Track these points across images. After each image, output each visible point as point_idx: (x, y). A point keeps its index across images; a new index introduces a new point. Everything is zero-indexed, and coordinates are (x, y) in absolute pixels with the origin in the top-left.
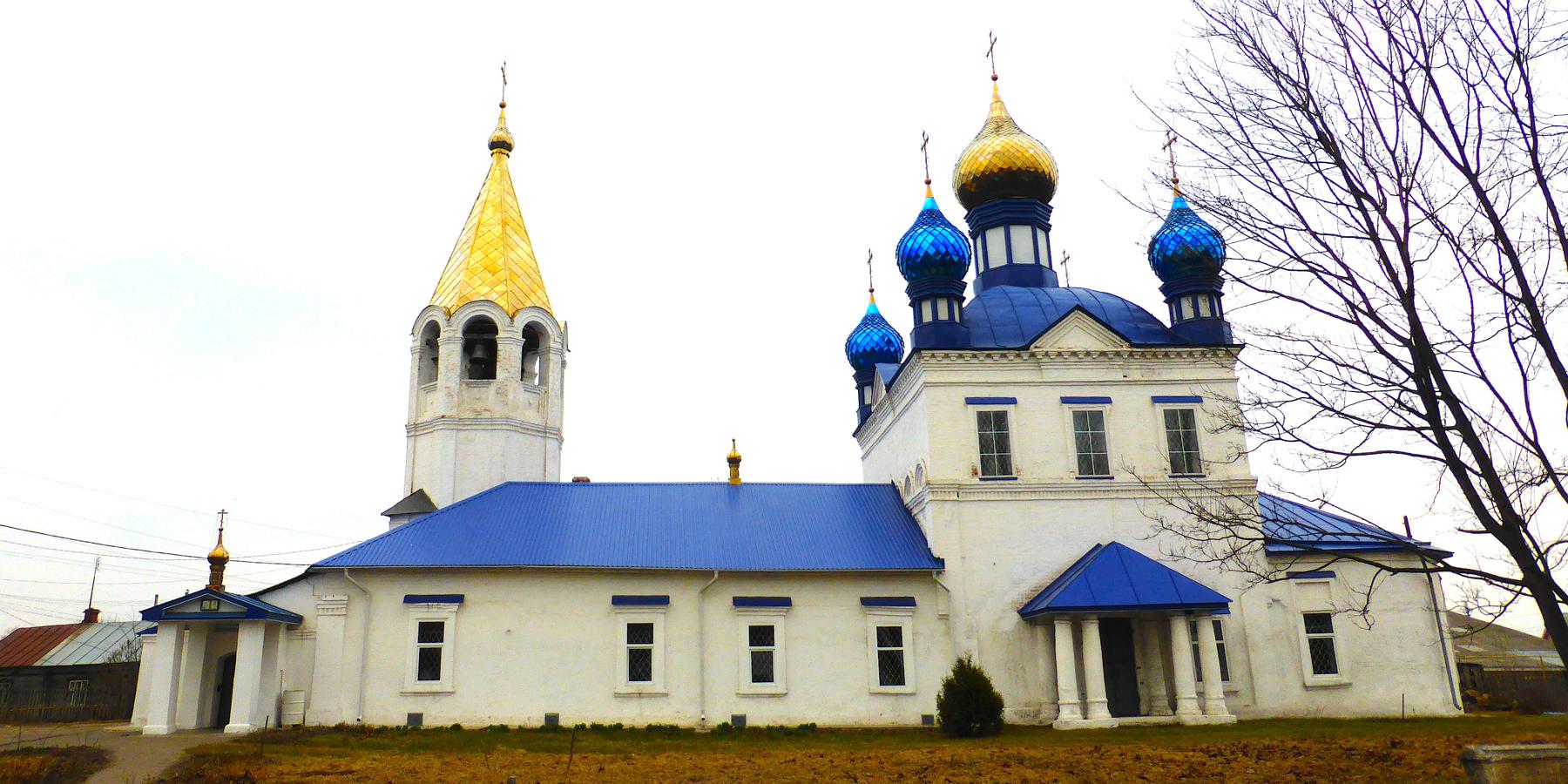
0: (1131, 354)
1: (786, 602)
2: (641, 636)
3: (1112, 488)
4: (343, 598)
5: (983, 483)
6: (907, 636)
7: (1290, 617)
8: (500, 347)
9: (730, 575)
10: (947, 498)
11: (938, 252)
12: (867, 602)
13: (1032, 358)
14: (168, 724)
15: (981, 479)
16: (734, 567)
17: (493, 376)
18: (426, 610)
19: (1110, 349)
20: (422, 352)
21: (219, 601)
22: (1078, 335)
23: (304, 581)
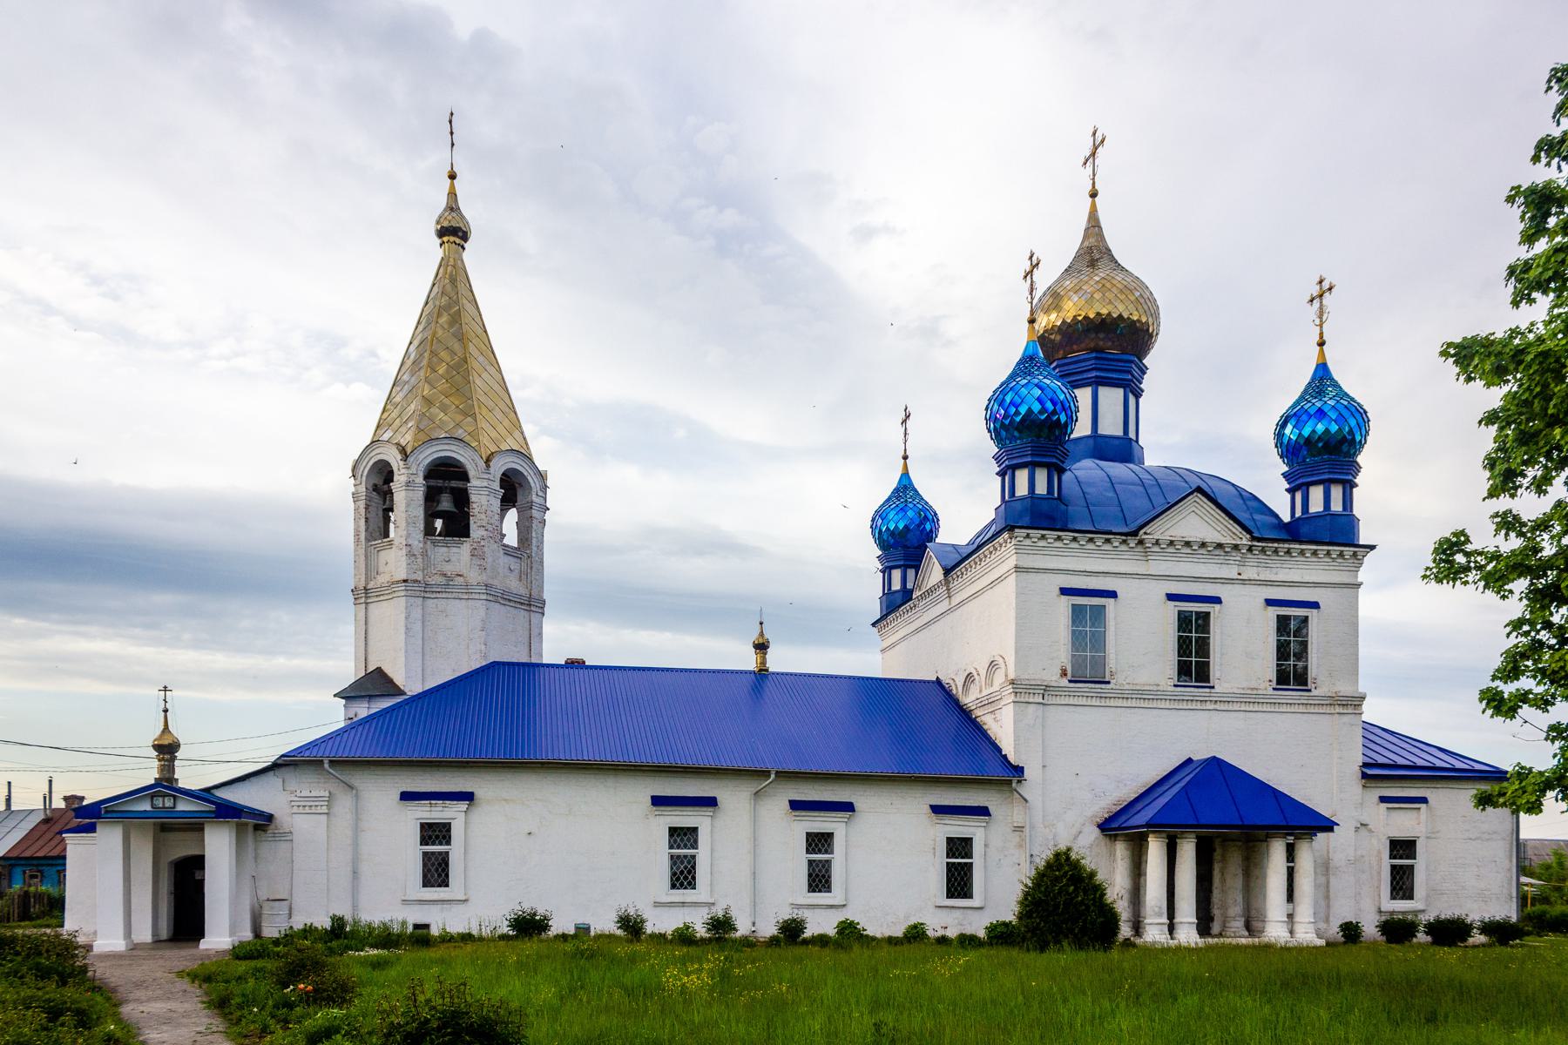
0: (1250, 549)
1: (848, 807)
2: (682, 840)
3: (1211, 699)
4: (322, 794)
5: (1072, 685)
6: (977, 848)
7: (1375, 841)
8: (473, 498)
9: (786, 776)
10: (1031, 700)
11: (1044, 410)
12: (938, 810)
13: (1139, 546)
14: (125, 939)
15: (1070, 681)
16: (792, 767)
17: (468, 536)
18: (428, 809)
19: (1228, 542)
20: (369, 500)
21: (174, 797)
22: (1195, 522)
23: (271, 773)
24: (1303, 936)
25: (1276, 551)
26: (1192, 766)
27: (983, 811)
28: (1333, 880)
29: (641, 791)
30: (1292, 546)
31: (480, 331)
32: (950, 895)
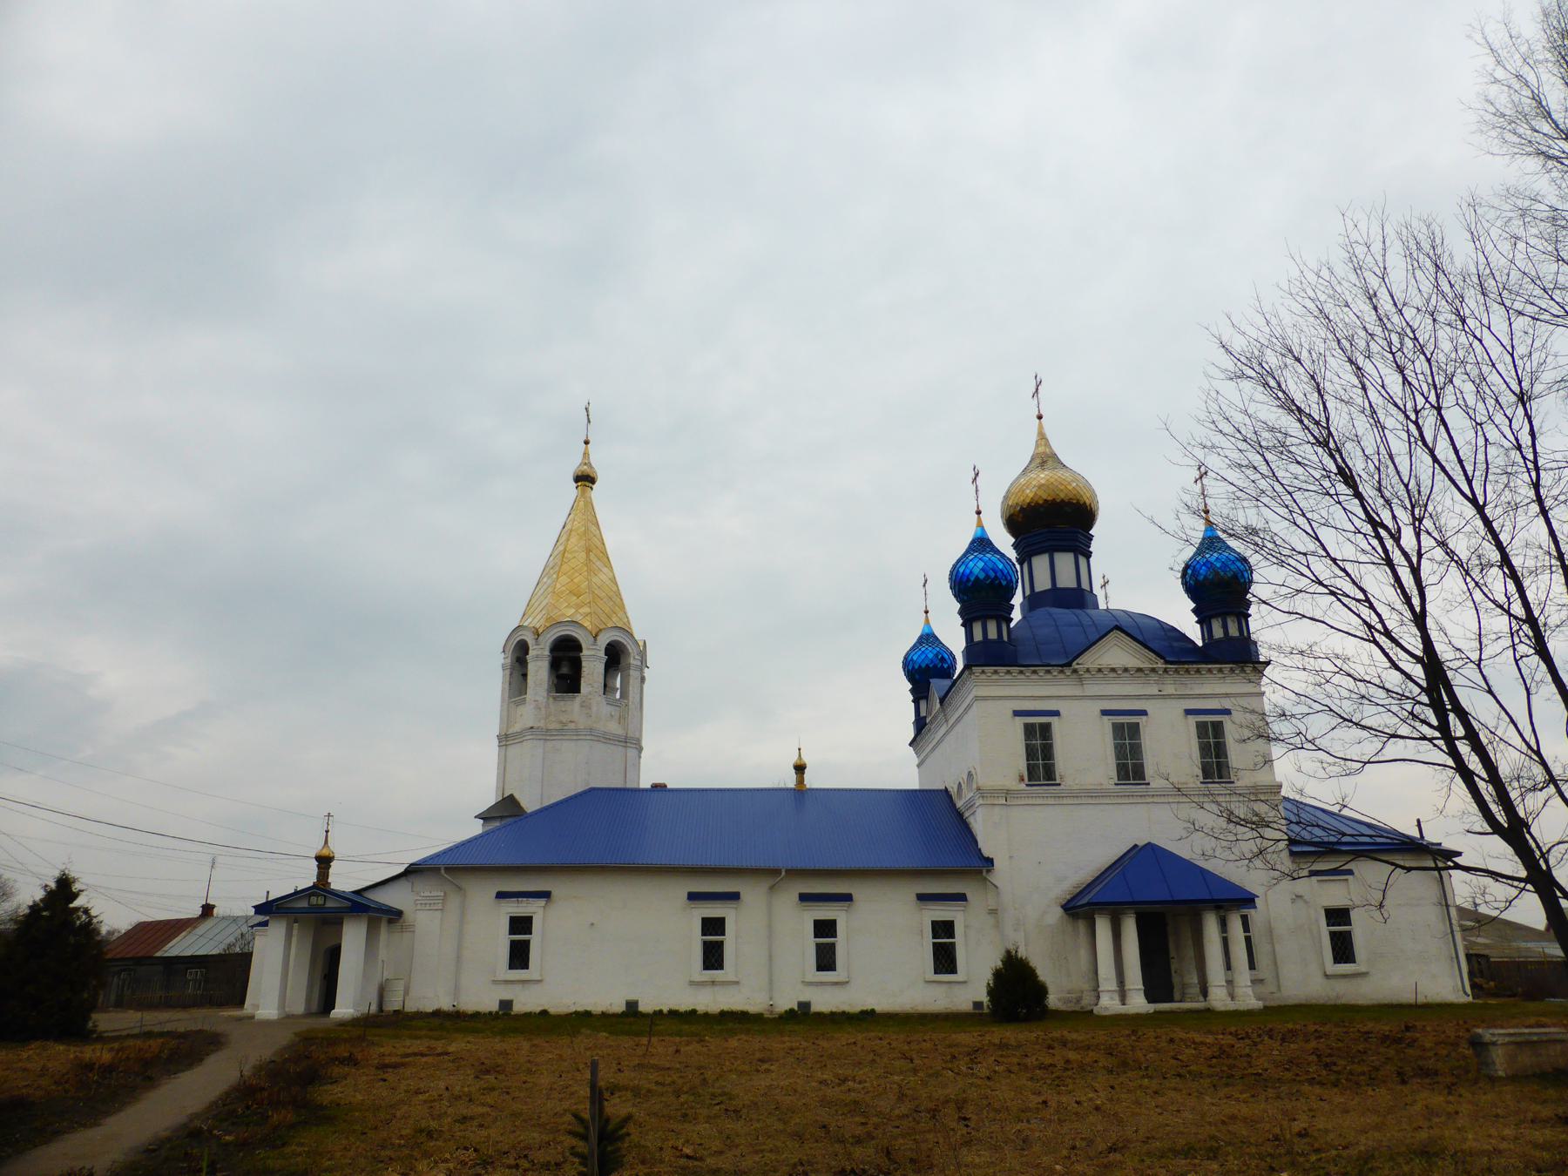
0: (1165, 671)
4: (439, 894)
6: (959, 930)
8: (584, 664)
22: (1116, 653)
23: (404, 878)
24: (1105, 1003)
25: (1187, 671)
26: (1137, 849)
27: (961, 897)
28: (1277, 947)
29: (679, 889)
30: (1199, 666)
31: (598, 544)
32: (512, 966)
